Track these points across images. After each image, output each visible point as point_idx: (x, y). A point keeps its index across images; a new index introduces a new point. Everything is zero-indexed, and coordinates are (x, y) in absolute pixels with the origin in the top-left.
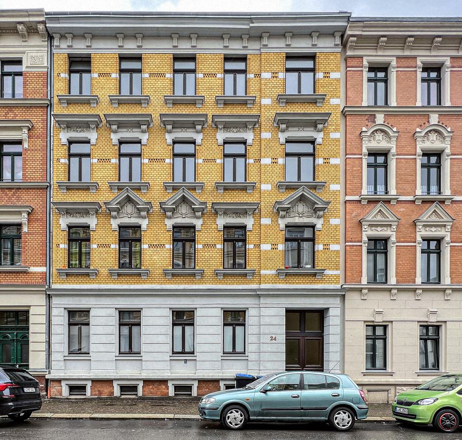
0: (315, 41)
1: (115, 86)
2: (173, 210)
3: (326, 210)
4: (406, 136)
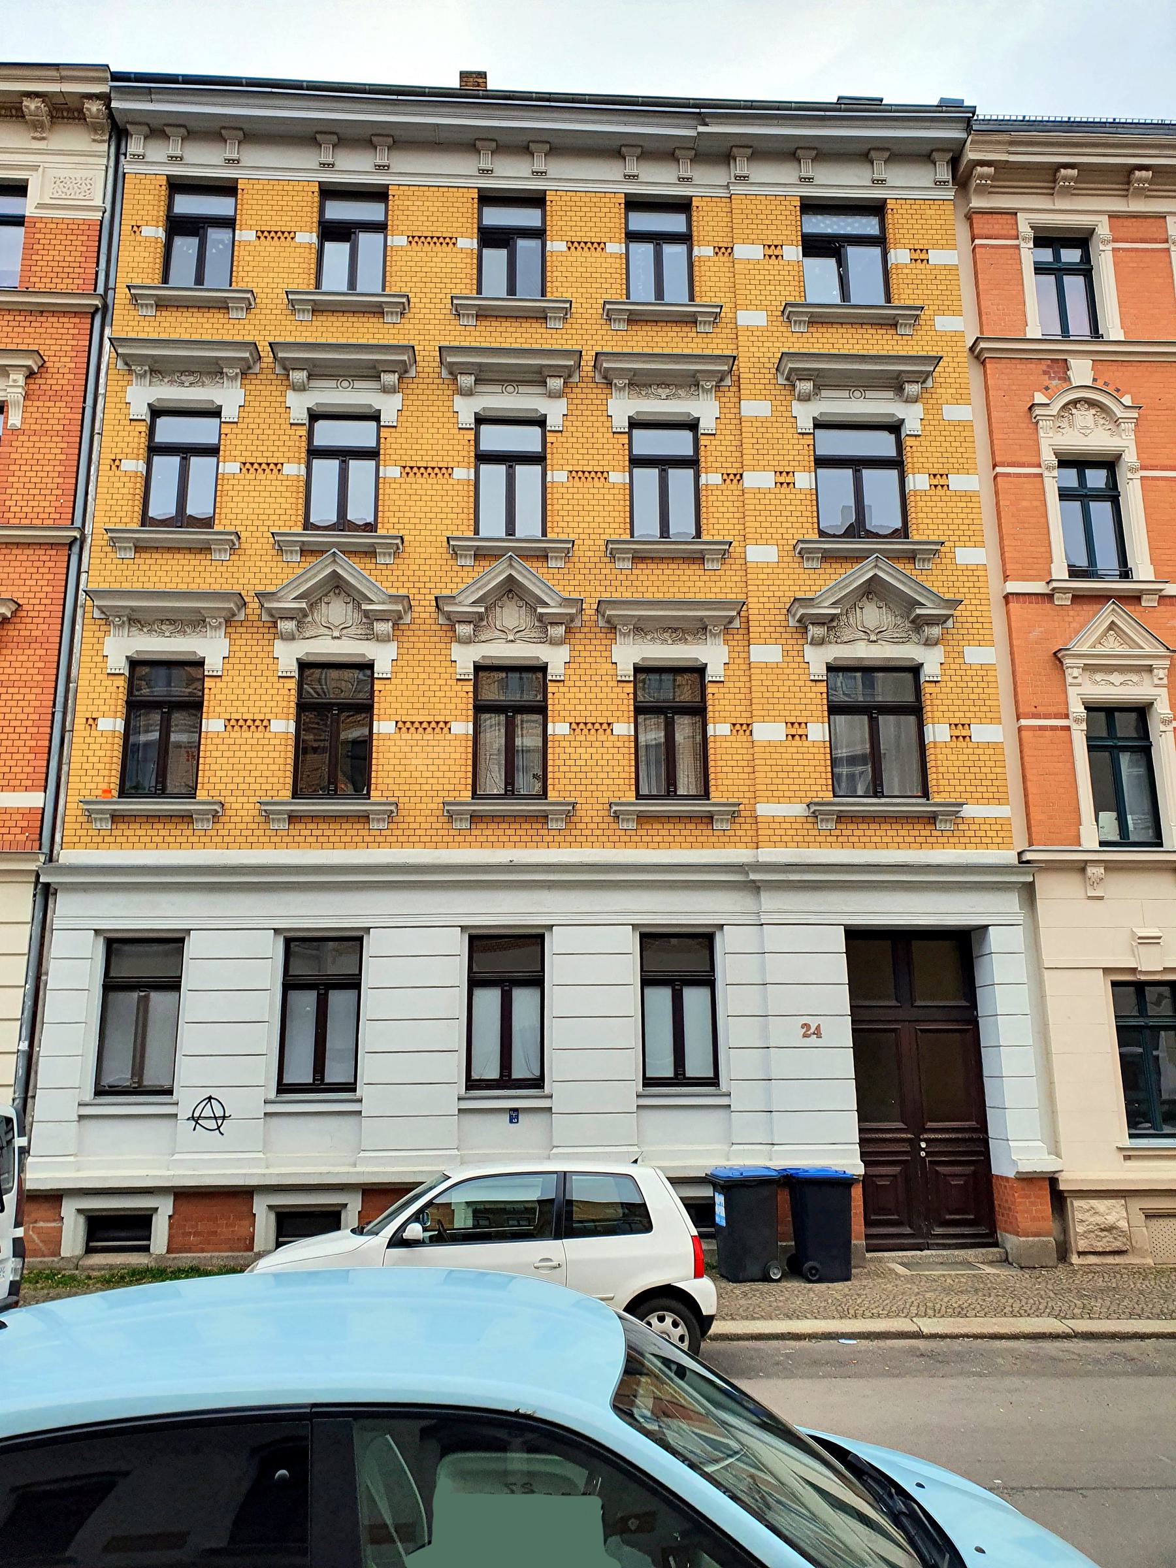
0: (881, 170)
1: (305, 265)
2: (477, 621)
3: (950, 623)
4: (1162, 418)
